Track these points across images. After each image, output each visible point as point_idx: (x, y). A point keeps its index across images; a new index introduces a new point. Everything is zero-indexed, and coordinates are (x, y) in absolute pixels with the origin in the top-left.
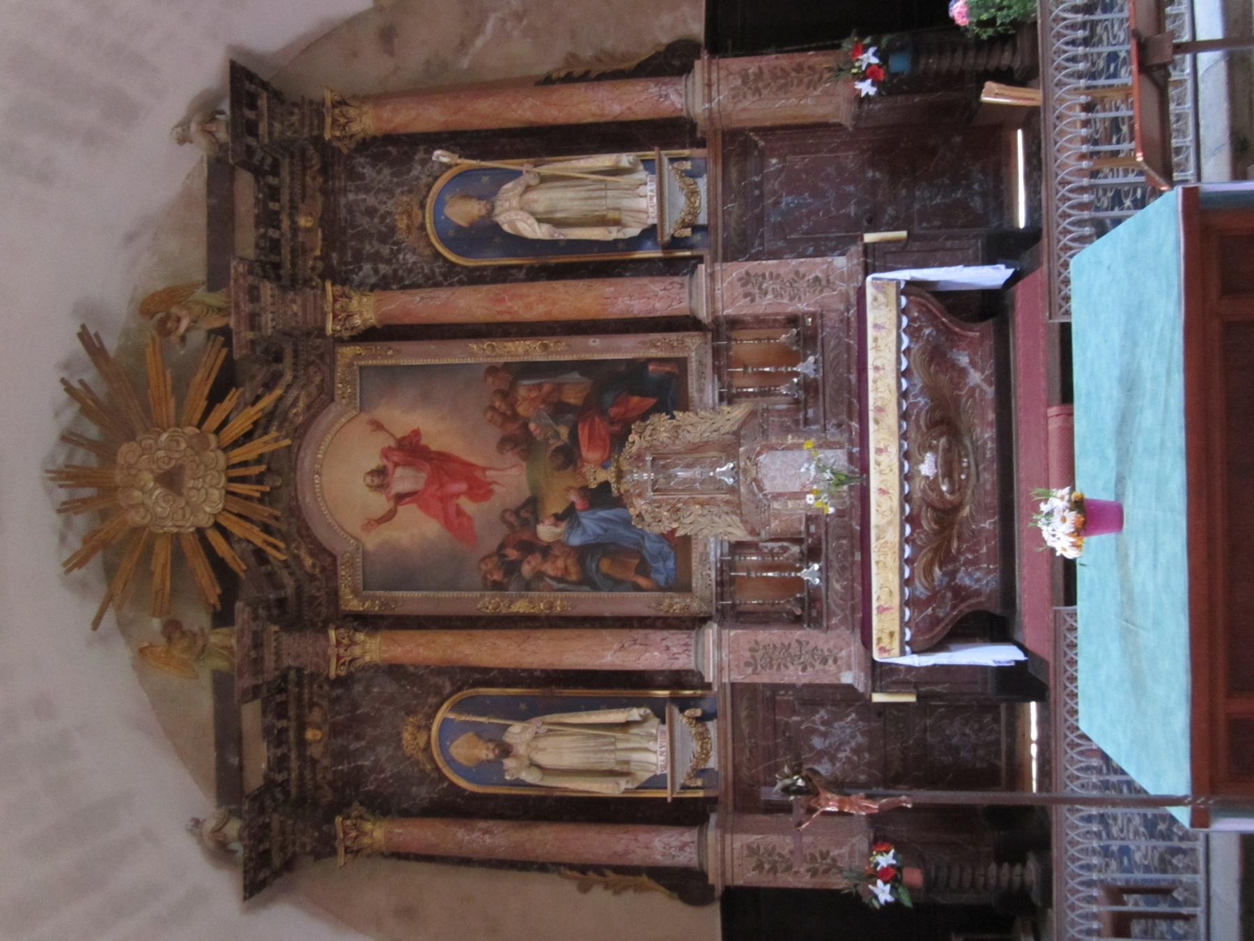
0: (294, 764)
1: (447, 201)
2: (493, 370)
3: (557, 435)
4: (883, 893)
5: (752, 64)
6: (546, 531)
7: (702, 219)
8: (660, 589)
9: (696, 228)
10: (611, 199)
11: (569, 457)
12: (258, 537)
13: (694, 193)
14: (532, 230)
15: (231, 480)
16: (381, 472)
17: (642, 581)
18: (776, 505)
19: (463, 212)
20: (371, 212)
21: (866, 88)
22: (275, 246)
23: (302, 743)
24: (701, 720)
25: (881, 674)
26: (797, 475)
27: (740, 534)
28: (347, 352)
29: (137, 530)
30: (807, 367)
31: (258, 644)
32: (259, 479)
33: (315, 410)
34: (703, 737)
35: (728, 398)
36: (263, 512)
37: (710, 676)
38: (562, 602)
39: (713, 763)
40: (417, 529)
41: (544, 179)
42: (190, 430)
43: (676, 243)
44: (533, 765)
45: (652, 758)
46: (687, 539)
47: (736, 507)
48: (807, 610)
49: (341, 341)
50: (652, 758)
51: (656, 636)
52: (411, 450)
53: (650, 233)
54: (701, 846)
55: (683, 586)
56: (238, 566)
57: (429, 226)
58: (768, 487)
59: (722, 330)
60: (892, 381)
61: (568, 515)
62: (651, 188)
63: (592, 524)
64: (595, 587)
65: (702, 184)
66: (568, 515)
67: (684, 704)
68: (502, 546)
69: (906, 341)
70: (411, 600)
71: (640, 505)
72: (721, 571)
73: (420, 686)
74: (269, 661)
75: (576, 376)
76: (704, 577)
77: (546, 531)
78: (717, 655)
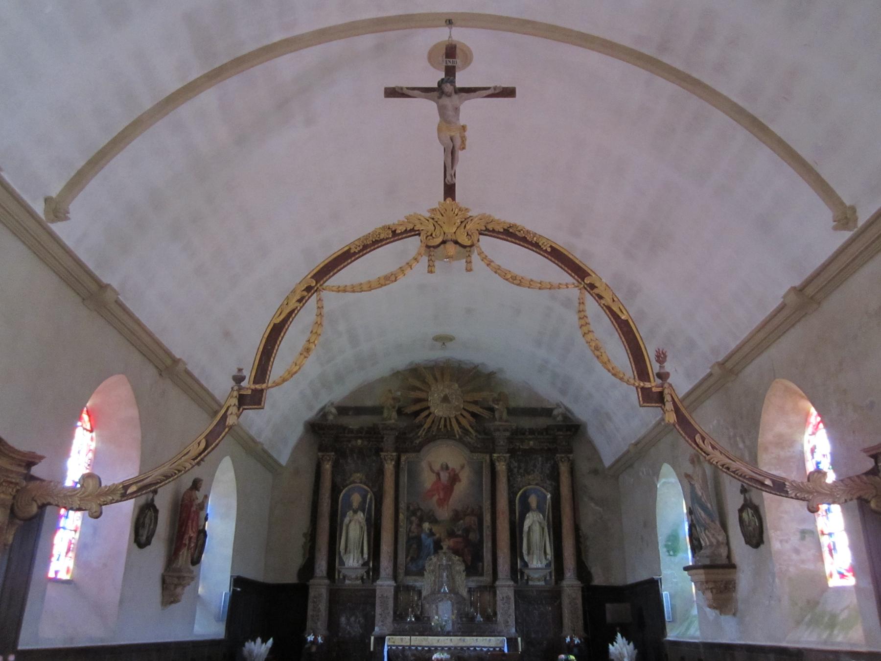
0: (350, 435)
1: (539, 494)
2: (481, 508)
3: (458, 530)
4: (311, 638)
5: (579, 601)
6: (426, 526)
7: (531, 583)
8: (406, 567)
9: (527, 580)
10: (537, 552)
11: (451, 534)
12: (426, 426)
13: (539, 580)
14: (527, 524)
15: (445, 419)
16: (447, 468)
17: (409, 558)
18: (434, 606)
19: (533, 500)
20: (535, 466)
21: (568, 639)
22: (524, 434)
23: (357, 438)
24: (362, 578)
25: (380, 640)
26: (443, 613)
27: (424, 593)
28: (488, 457)
29: (430, 387)
30: (479, 618)
31: (392, 429)
32: (445, 426)
33: (467, 445)
34: (357, 578)
35: (470, 591)
36: (435, 428)
37: (379, 582)
38: (402, 530)
39: (347, 582)
40: (428, 480)
41: (543, 529)
42: (462, 406)
43: (522, 574)
44: (350, 521)
45: (351, 561)
46: (423, 575)
47: (433, 593)
48: (399, 616)
49: (491, 457)
50: (351, 561)
51: (391, 564)
52: (454, 479)
53: (526, 565)
54: (321, 578)
55: (407, 573)
56: (417, 421)
57: (529, 487)
58: (440, 604)
59: (492, 588)
60: (473, 644)
61: (431, 534)
62: (540, 566)
63: (428, 542)
64: (407, 543)
65: (542, 583)
66: (431, 534)
67: (368, 573)
68: (422, 510)
69: (485, 649)
70: (404, 479)
71: (434, 559)
72: (411, 586)
73: (376, 480)
74: (385, 432)
75: (478, 537)
76: (410, 581)
77: (426, 526)
78: (385, 585)
